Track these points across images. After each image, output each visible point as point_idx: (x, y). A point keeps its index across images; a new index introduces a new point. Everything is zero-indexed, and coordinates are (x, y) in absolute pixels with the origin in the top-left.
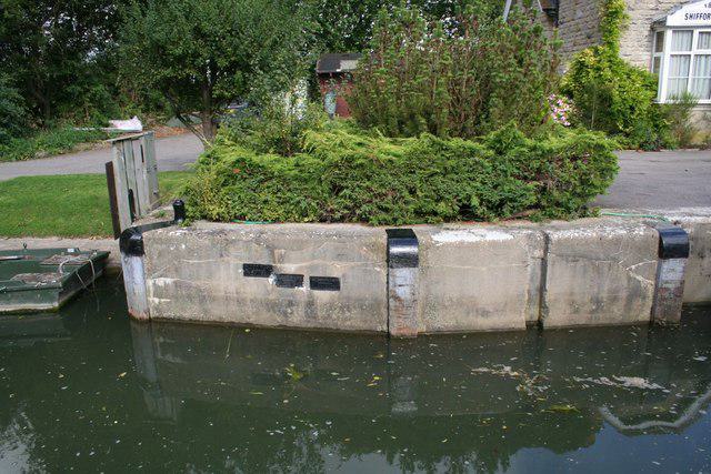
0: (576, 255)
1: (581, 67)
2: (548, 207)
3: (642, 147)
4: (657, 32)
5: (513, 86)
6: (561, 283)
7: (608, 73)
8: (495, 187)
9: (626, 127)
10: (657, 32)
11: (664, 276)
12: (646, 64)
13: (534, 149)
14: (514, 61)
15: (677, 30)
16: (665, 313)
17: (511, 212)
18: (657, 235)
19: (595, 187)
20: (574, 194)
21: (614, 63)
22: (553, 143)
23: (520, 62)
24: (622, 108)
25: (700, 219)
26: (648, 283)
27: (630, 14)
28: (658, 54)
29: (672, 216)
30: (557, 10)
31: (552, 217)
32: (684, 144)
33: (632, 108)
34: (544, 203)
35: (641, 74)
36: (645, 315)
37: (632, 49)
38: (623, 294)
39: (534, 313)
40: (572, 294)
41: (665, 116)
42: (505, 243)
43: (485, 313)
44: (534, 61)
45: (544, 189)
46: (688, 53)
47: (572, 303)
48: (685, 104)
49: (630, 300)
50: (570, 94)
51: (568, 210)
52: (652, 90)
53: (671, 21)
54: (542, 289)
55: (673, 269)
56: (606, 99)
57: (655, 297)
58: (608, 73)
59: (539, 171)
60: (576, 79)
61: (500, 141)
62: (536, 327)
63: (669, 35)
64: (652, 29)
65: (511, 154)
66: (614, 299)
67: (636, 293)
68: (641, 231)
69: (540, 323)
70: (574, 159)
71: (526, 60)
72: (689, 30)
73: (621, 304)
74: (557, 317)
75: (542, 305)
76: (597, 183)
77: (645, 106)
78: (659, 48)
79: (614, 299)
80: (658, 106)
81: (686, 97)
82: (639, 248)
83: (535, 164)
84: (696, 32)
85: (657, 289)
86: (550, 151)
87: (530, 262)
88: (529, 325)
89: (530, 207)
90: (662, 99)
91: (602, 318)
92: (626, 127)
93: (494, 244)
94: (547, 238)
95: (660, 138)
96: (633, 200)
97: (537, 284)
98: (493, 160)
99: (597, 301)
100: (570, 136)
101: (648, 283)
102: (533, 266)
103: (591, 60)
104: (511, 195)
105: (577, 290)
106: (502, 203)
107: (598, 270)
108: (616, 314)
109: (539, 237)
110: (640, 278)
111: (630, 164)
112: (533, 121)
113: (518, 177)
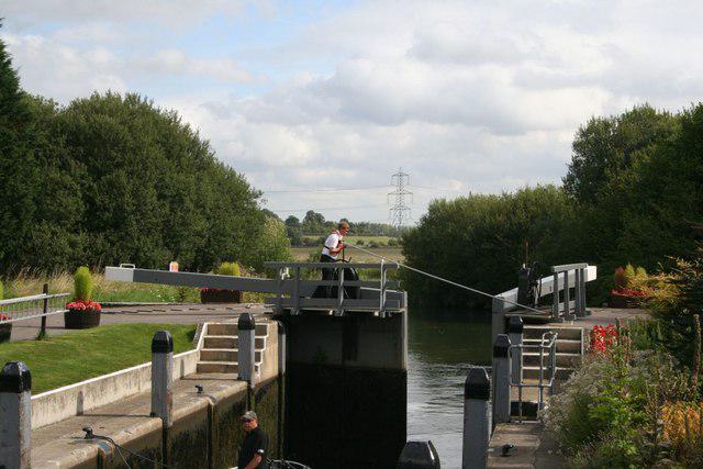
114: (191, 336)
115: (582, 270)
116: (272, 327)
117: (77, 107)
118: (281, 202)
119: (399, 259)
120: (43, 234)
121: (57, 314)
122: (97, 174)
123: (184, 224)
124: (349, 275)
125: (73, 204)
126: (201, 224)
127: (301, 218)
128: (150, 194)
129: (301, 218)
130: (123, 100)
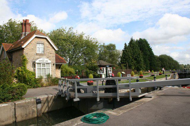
0: (21, 106)
1: (19, 71)
2: (13, 99)
3: (34, 87)
4: (34, 64)
5: (5, 76)
6: (19, 112)
7: (24, 72)
8: (3, 96)
9: (30, 83)
10: (34, 64)
11: (38, 107)
12: (33, 70)
13: (11, 87)
14: (5, 71)
15: (38, 63)
16: (39, 114)
17: (7, 101)
18: (35, 100)
19: (23, 93)
20: (20, 95)
21: (25, 70)
22: (14, 86)
23: (6, 71)
24: (29, 80)
25: (43, 97)
26: (35, 109)
27: (28, 60)
28: (35, 68)
29: (38, 98)
30: (12, 59)
31: (16, 100)
32: (42, 86)
33: (30, 80)
34: (14, 98)
35: (32, 72)
36: (36, 116)
37: (29, 67)
38: (31, 112)
39: (14, 120)
40: (21, 114)
41: (38, 81)
42: (7, 106)
43: (3, 122)
44: (9, 71)
45: (13, 95)
46: (45, 68)
47: (21, 116)
48: (41, 78)
49: (33, 113)
50: (16, 77)
51: (19, 99)
52: (34, 76)
53: (36, 62)
54: (15, 114)
55: (39, 106)
56: (24, 78)
57: (37, 112)
58: (24, 72)
59: (12, 91)
60: (18, 74)
61: (3, 87)
62: (15, 122)
63: (36, 65)
64: (33, 63)
65: (6, 89)
66: (30, 113)
67: (33, 112)
68: (33, 100)
69: (15, 121)
70: (19, 88)
71: (7, 71)
72: (40, 64)
73: (31, 114)
74: (19, 119)
75: (16, 118)
76: (24, 93)
77: (34, 79)
78: (35, 67)
79: (30, 113)
80: (36, 79)
81: (41, 77)
82: (33, 103)
83: (11, 90)
84: (41, 64)
85: (37, 110)
86: (14, 87)
87: (12, 109)
88: (13, 122)
89: (11, 99)
90: (37, 77)
91: (28, 118)
92: (30, 83)
93: (4, 106)
94: (15, 104)
95: (37, 85)
96: (30, 96)
97: (14, 114)
98: (2, 90)
99: (26, 114)
100: (17, 85)
101: (35, 109)
102: (13, 110)
103: (20, 70)
104: (6, 97)
105: (22, 113)
106: (5, 99)
107: (26, 108)
108: (31, 116)
109: (13, 104)
110: (34, 109)
111: (30, 91)
112: (10, 83)
113: (8, 93)
114: (170, 76)
115: (132, 96)
116: (177, 75)
117: (160, 56)
118: (181, 62)
119: (23, 47)
120: (157, 68)
121: (158, 74)
122: (162, 62)
123: (171, 66)
124: (184, 70)
125: (160, 65)
126: (173, 66)
127: (187, 65)
128: (167, 63)
129: (187, 65)
130: (127, 46)
